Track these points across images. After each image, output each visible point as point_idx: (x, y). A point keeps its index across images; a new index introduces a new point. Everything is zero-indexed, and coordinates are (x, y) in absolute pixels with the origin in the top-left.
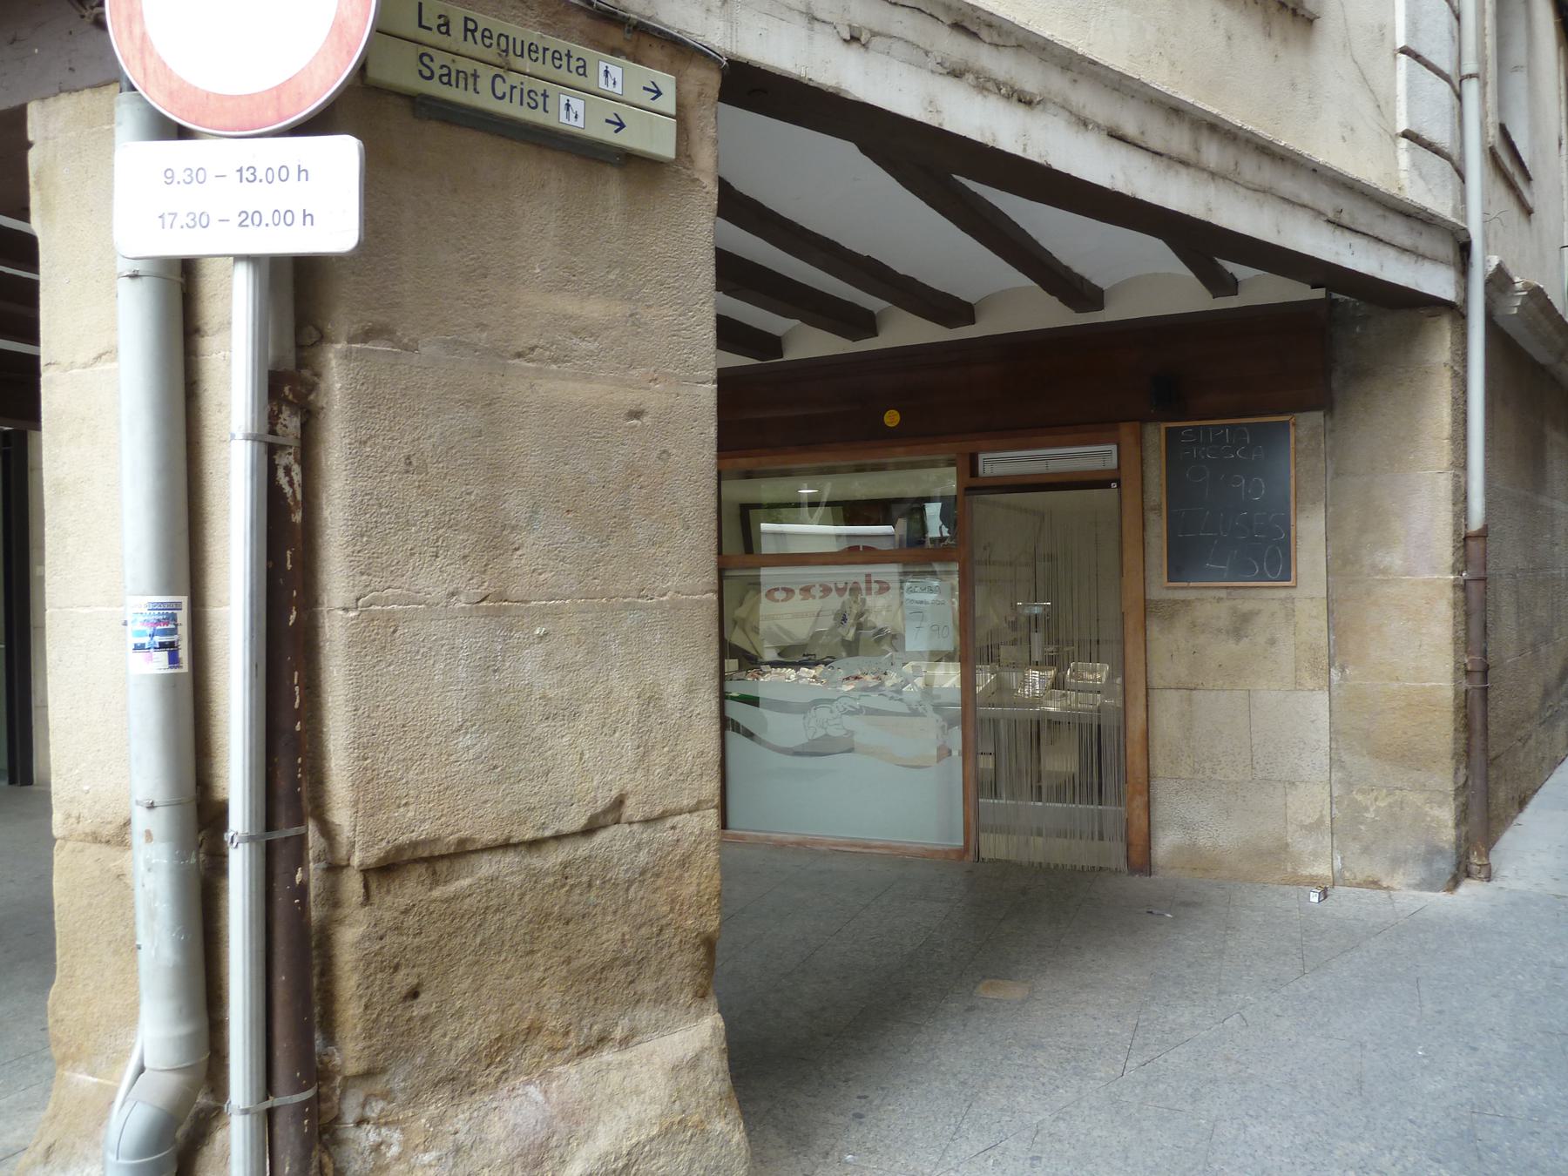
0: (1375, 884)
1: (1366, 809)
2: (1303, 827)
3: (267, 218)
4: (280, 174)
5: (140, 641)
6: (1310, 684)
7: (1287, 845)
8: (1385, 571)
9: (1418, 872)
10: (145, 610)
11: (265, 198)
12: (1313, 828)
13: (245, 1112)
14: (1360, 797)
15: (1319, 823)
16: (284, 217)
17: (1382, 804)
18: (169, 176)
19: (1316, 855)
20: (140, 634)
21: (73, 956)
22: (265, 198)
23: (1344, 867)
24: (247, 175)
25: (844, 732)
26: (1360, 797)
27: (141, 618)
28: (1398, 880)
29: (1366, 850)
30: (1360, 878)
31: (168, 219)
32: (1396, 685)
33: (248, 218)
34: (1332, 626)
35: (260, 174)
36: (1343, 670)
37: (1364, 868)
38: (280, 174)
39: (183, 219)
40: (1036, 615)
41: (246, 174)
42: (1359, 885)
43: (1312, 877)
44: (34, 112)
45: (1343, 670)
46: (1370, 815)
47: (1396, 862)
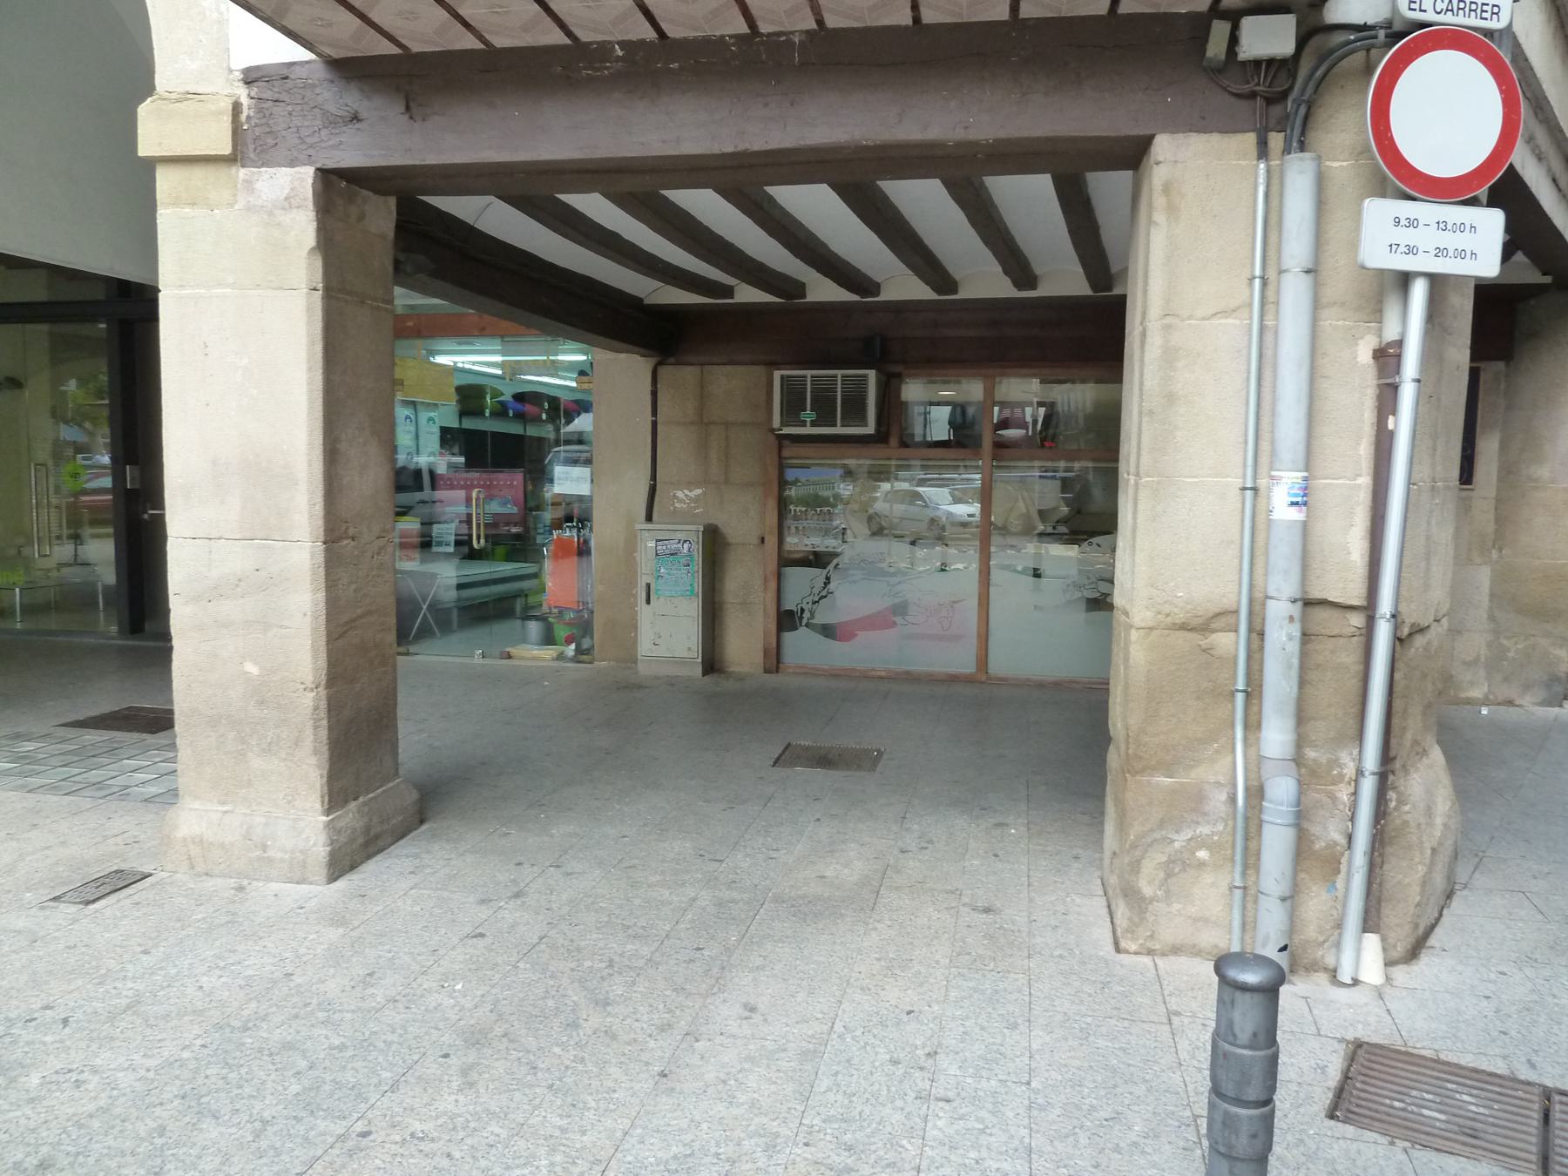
0: (1510, 703)
1: (1509, 650)
2: (1465, 663)
3: (1451, 254)
4: (1461, 228)
5: (1295, 500)
6: (1478, 560)
7: (1452, 676)
8: (1536, 480)
9: (1541, 694)
10: (1300, 481)
11: (1451, 241)
12: (1472, 664)
13: (1374, 774)
14: (1505, 642)
15: (1476, 661)
16: (1461, 254)
17: (1520, 646)
18: (1397, 222)
19: (1472, 684)
20: (1296, 495)
21: (1158, 703)
22: (1451, 241)
23: (1489, 691)
24: (1442, 226)
25: (1099, 594)
26: (1505, 642)
27: (1297, 486)
28: (1527, 700)
29: (1506, 679)
30: (1500, 699)
31: (1394, 247)
32: (1537, 562)
33: (1440, 252)
34: (1497, 520)
35: (1449, 227)
36: (1500, 550)
37: (1505, 692)
38: (1461, 228)
39: (1402, 249)
40: (422, 524)
41: (1442, 226)
42: (1499, 704)
43: (1468, 698)
44: (1164, 147)
45: (1500, 550)
46: (1510, 655)
47: (1527, 687)
